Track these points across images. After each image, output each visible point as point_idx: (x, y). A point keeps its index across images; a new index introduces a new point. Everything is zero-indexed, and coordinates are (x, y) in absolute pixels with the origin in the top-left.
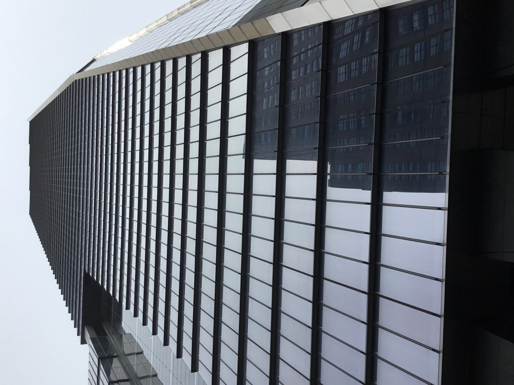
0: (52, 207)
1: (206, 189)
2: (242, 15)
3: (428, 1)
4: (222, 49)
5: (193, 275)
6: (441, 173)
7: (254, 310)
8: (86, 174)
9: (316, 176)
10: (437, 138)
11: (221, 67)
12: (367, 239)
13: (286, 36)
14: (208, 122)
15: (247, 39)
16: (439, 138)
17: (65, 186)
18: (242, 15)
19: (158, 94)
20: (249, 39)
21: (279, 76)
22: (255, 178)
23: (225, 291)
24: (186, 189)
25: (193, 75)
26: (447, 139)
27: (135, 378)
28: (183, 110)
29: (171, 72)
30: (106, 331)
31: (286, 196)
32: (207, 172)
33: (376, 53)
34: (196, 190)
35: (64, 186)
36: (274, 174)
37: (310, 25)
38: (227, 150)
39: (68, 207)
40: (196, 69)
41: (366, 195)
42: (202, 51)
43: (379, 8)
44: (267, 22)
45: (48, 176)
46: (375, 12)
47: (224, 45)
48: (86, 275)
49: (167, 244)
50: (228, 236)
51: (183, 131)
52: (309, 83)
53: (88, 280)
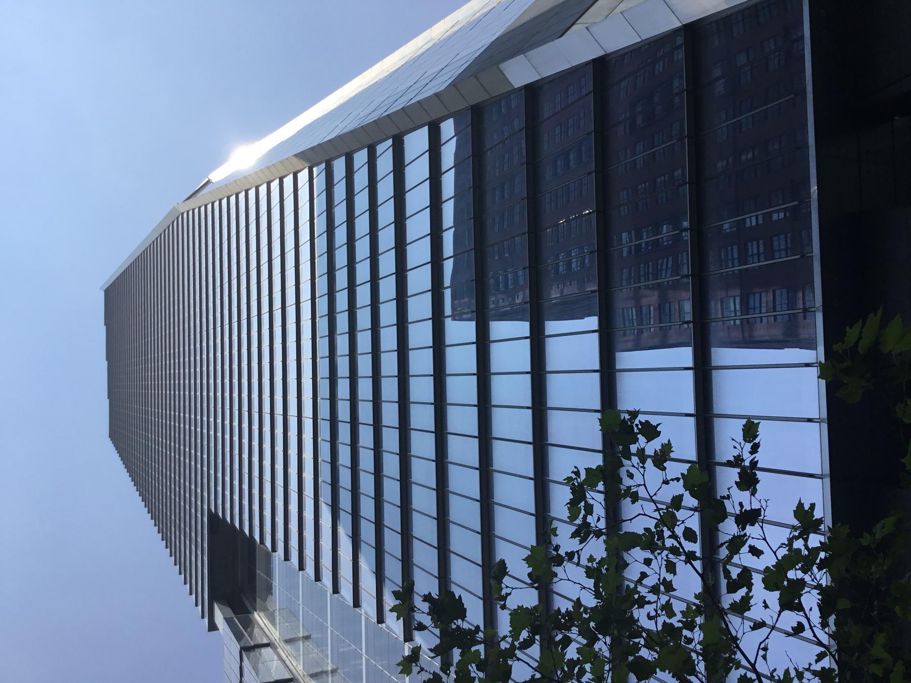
0: (148, 444)
1: (411, 400)
2: (455, 75)
3: (764, 1)
4: (426, 128)
5: (399, 565)
6: (806, 310)
7: (502, 455)
8: (205, 356)
9: (597, 334)
10: (790, 97)
11: (427, 153)
12: (689, 377)
13: (532, 91)
14: (381, 301)
15: (467, 102)
16: (792, 96)
17: (170, 411)
18: (455, 75)
19: (323, 232)
20: (471, 104)
21: (524, 145)
22: (414, 434)
23: (455, 562)
24: (378, 400)
25: (381, 199)
26: (809, 202)
27: (302, 675)
28: (367, 230)
29: (344, 174)
30: (249, 608)
31: (548, 406)
32: (411, 345)
33: (680, 46)
34: (397, 402)
35: (177, 424)
36: (526, 338)
37: (570, 66)
38: (440, 129)
39: (177, 446)
40: (385, 164)
41: (685, 355)
42: (393, 136)
43: (681, 25)
44: (502, 72)
45: (137, 402)
46: (676, 32)
47: (429, 120)
48: (213, 517)
49: (350, 488)
50: (417, 519)
51: (368, 286)
52: (574, 116)
53: (216, 524)
